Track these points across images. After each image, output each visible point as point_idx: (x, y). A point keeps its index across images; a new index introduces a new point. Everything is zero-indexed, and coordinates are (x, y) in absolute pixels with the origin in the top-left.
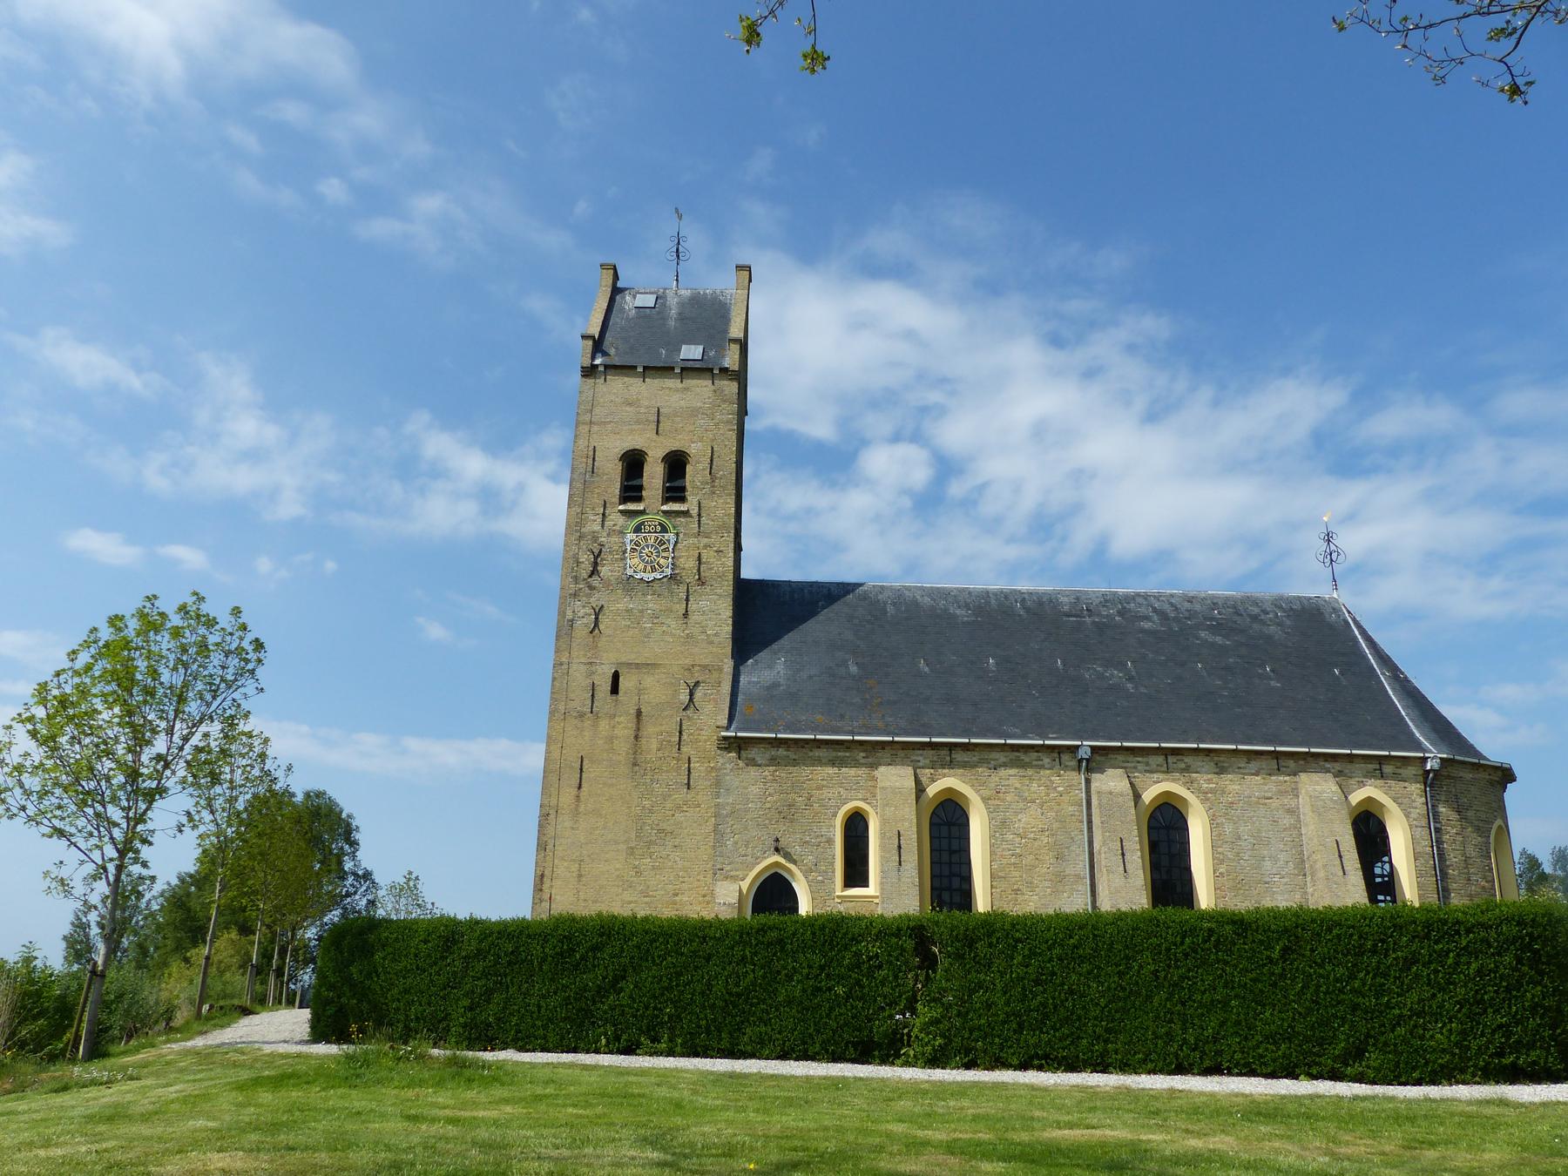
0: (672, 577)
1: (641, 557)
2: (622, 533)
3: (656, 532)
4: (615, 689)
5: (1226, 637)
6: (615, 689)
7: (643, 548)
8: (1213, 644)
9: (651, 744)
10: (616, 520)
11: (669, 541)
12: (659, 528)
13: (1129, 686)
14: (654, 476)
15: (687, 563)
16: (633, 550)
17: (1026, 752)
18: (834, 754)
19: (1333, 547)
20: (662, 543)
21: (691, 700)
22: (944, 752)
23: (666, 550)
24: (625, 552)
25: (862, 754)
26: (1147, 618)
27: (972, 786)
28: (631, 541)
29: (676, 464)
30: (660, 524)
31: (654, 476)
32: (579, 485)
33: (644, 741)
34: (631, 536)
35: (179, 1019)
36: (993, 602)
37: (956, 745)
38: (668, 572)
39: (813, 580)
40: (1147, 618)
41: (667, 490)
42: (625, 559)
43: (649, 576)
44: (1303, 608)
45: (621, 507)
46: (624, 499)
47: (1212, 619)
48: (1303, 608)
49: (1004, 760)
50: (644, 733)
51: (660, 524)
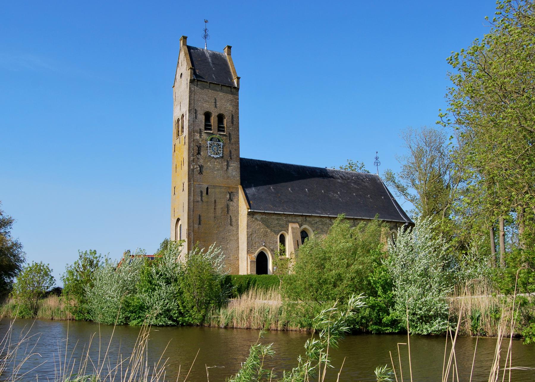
0: (222, 157)
1: (213, 149)
2: (207, 140)
3: (217, 141)
4: (207, 193)
5: (357, 186)
6: (207, 193)
7: (213, 146)
8: (355, 188)
9: (219, 211)
10: (204, 136)
11: (221, 145)
12: (218, 140)
13: (340, 199)
14: (213, 120)
15: (227, 153)
16: (210, 147)
17: (323, 218)
18: (277, 217)
19: (378, 161)
20: (219, 145)
21: (230, 198)
22: (304, 218)
23: (220, 148)
24: (207, 147)
25: (284, 218)
26: (338, 178)
27: (311, 227)
28: (209, 144)
29: (221, 118)
30: (218, 139)
31: (213, 120)
32: (192, 122)
33: (217, 210)
34: (209, 142)
35: (461, 327)
36: (301, 170)
37: (307, 216)
38: (221, 155)
39: (251, 159)
40: (338, 178)
41: (219, 127)
42: (207, 149)
43: (216, 156)
44: (372, 178)
45: (206, 131)
46: (206, 129)
47: (353, 180)
48: (372, 178)
49: (318, 220)
50: (217, 207)
51: (218, 139)
